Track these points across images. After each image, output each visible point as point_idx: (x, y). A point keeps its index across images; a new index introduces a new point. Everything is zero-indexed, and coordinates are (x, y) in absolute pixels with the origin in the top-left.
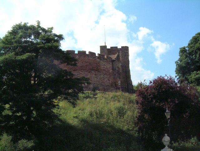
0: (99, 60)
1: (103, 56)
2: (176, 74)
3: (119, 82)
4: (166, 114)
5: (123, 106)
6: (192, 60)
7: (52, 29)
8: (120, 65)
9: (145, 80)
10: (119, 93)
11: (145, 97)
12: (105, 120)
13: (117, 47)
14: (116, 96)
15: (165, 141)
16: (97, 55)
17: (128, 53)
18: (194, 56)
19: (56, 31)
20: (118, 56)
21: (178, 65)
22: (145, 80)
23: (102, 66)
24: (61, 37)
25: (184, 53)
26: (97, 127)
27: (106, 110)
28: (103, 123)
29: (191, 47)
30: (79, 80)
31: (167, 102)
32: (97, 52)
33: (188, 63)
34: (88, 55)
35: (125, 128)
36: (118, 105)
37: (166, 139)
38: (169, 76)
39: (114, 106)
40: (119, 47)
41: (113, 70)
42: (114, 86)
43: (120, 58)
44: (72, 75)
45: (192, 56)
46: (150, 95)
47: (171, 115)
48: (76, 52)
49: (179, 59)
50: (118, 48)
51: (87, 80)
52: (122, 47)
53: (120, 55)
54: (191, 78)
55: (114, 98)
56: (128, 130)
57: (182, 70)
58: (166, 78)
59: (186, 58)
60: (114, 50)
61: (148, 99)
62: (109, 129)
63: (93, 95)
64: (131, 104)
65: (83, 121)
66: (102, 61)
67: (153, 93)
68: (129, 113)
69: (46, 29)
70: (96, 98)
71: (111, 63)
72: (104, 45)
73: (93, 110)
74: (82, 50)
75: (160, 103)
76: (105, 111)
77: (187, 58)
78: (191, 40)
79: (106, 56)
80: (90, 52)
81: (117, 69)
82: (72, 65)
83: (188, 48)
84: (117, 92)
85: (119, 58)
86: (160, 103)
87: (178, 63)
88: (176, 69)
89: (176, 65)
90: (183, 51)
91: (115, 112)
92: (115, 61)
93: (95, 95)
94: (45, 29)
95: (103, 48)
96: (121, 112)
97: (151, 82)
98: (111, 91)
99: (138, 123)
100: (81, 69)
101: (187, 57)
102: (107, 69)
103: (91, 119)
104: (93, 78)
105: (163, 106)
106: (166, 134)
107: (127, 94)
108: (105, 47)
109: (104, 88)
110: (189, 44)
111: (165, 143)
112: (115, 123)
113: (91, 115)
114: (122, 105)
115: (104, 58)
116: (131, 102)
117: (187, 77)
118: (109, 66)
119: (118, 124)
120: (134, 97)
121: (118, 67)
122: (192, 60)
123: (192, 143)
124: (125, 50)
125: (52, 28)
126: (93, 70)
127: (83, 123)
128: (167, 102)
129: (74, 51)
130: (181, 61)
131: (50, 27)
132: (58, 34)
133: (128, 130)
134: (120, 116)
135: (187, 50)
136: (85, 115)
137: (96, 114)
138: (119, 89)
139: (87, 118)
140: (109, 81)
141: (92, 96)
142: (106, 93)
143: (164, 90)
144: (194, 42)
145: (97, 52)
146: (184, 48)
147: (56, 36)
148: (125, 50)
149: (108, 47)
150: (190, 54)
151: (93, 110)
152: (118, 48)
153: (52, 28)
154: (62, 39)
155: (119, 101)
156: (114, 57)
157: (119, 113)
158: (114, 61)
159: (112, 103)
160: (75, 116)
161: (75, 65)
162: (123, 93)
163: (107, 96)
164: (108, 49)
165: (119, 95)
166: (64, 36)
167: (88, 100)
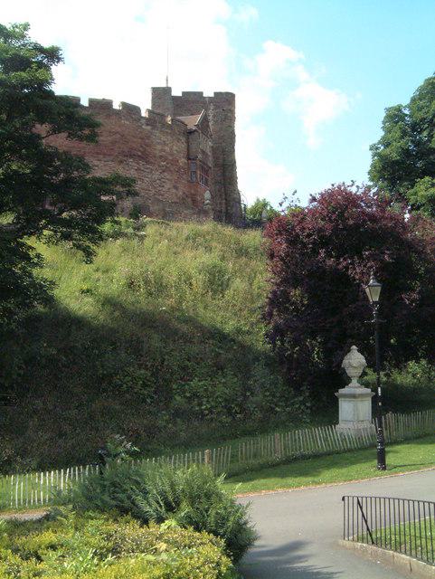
0: (149, 128)
1: (163, 116)
2: (372, 180)
3: (207, 195)
4: (367, 290)
5: (220, 262)
6: (418, 144)
7: (25, 29)
8: (208, 145)
9: (296, 192)
10: (208, 226)
11: (293, 241)
12: (172, 302)
13: (202, 93)
14: (197, 235)
15: (351, 365)
16: (144, 114)
17: (232, 112)
18: (425, 133)
19: (41, 36)
20: (205, 120)
21: (379, 155)
22: (296, 192)
23: (159, 147)
24: (53, 55)
25: (398, 122)
26: (148, 321)
27: (175, 274)
28: (165, 312)
29: (420, 109)
30: (105, 183)
31: (361, 257)
32: (145, 104)
33: (406, 153)
34: (117, 113)
35: (229, 327)
36: (208, 259)
37: (355, 360)
38: (361, 186)
39: (195, 261)
40: (208, 93)
41: (189, 159)
42: (192, 206)
43: (210, 124)
44: (87, 168)
45: (420, 133)
46: (309, 236)
47: (382, 293)
48: (85, 103)
49: (383, 138)
50: (204, 95)
51: (128, 183)
52: (183, 93)
53: (210, 118)
54: (416, 194)
55: (194, 241)
56: (239, 331)
57: (392, 170)
58: (354, 190)
59: (402, 137)
60: (191, 101)
61: (304, 245)
62: (185, 328)
63: (134, 229)
64: (244, 259)
65: (109, 302)
66: (157, 133)
67: (320, 230)
68: (238, 284)
69: (8, 27)
70: (142, 238)
71: (183, 139)
72: (164, 85)
73: (137, 272)
74: (218, 91)
75: (338, 258)
76: (171, 276)
77: (407, 138)
78: (421, 89)
79: (169, 118)
80: (124, 105)
81: (200, 156)
82: (81, 139)
83: (410, 109)
84: (201, 223)
85: (208, 126)
86: (338, 258)
87: (377, 149)
88: (373, 166)
89: (374, 156)
90: (394, 116)
91: (199, 280)
92: (197, 135)
93: (138, 229)
94: (5, 29)
95: (160, 94)
96: (217, 282)
97: (314, 199)
98: (185, 219)
99: (271, 315)
100: (98, 153)
101: (404, 133)
102: (172, 155)
103: (131, 298)
104: (149, 181)
105: (347, 268)
106: (354, 347)
107: (229, 231)
108: (167, 90)
109: (164, 210)
110: (413, 100)
111: (350, 372)
112: (201, 311)
113: (131, 285)
114: (218, 262)
115: (164, 124)
116: (242, 252)
117: (402, 190)
118: (177, 147)
119: (209, 314)
120: (254, 238)
121: (202, 150)
122: (418, 144)
123: (414, 376)
124: (225, 103)
125: (26, 27)
126: (131, 156)
127: (108, 308)
128: (361, 257)
129: (78, 100)
130: (387, 145)
131: (22, 21)
132: (46, 45)
133: (239, 331)
134: (215, 292)
135: (406, 115)
136: (114, 286)
137: (147, 282)
138: (206, 213)
139: (119, 296)
140: (174, 191)
141: (130, 230)
142: (172, 224)
143: (351, 222)
144: (428, 93)
145: (145, 104)
146: (399, 109)
147: (39, 49)
148: (225, 103)
149: (176, 92)
150: (415, 127)
151: (137, 272)
152: (204, 95)
153: (26, 27)
154: (58, 62)
155: (209, 249)
156: (193, 121)
157: (211, 282)
158: (191, 132)
159: (189, 254)
160: (85, 288)
161: (92, 138)
162: (219, 226)
163: (174, 232)
164: (175, 98)
165: (208, 233)
166: (64, 53)
167: (119, 242)
